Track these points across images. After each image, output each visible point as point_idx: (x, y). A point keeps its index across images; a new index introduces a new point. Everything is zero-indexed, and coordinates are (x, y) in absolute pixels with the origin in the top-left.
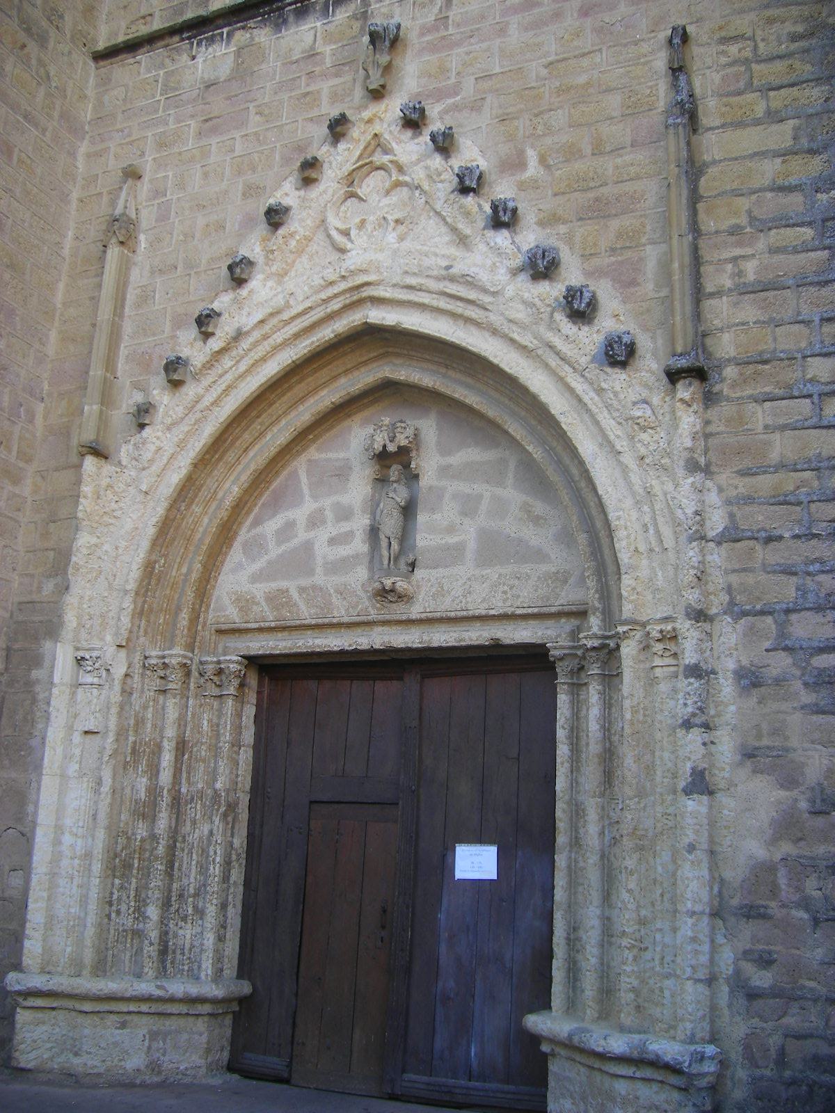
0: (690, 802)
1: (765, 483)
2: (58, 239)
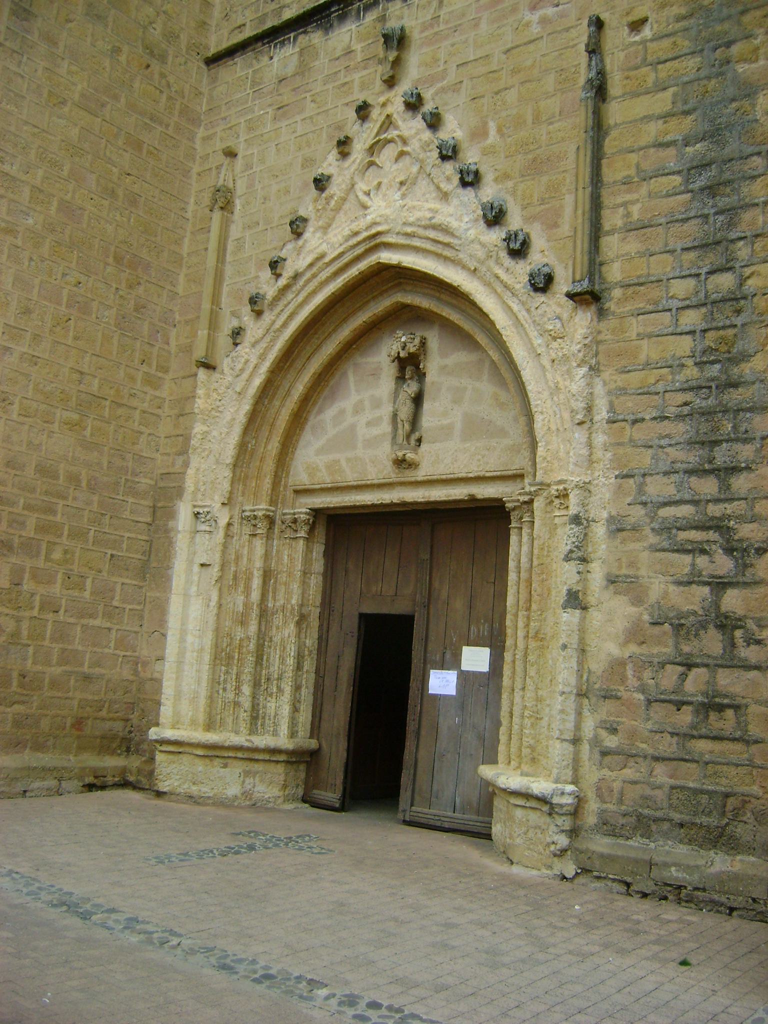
0: (565, 614)
1: (635, 379)
2: (183, 206)
